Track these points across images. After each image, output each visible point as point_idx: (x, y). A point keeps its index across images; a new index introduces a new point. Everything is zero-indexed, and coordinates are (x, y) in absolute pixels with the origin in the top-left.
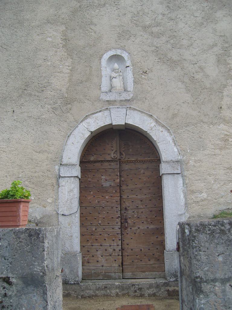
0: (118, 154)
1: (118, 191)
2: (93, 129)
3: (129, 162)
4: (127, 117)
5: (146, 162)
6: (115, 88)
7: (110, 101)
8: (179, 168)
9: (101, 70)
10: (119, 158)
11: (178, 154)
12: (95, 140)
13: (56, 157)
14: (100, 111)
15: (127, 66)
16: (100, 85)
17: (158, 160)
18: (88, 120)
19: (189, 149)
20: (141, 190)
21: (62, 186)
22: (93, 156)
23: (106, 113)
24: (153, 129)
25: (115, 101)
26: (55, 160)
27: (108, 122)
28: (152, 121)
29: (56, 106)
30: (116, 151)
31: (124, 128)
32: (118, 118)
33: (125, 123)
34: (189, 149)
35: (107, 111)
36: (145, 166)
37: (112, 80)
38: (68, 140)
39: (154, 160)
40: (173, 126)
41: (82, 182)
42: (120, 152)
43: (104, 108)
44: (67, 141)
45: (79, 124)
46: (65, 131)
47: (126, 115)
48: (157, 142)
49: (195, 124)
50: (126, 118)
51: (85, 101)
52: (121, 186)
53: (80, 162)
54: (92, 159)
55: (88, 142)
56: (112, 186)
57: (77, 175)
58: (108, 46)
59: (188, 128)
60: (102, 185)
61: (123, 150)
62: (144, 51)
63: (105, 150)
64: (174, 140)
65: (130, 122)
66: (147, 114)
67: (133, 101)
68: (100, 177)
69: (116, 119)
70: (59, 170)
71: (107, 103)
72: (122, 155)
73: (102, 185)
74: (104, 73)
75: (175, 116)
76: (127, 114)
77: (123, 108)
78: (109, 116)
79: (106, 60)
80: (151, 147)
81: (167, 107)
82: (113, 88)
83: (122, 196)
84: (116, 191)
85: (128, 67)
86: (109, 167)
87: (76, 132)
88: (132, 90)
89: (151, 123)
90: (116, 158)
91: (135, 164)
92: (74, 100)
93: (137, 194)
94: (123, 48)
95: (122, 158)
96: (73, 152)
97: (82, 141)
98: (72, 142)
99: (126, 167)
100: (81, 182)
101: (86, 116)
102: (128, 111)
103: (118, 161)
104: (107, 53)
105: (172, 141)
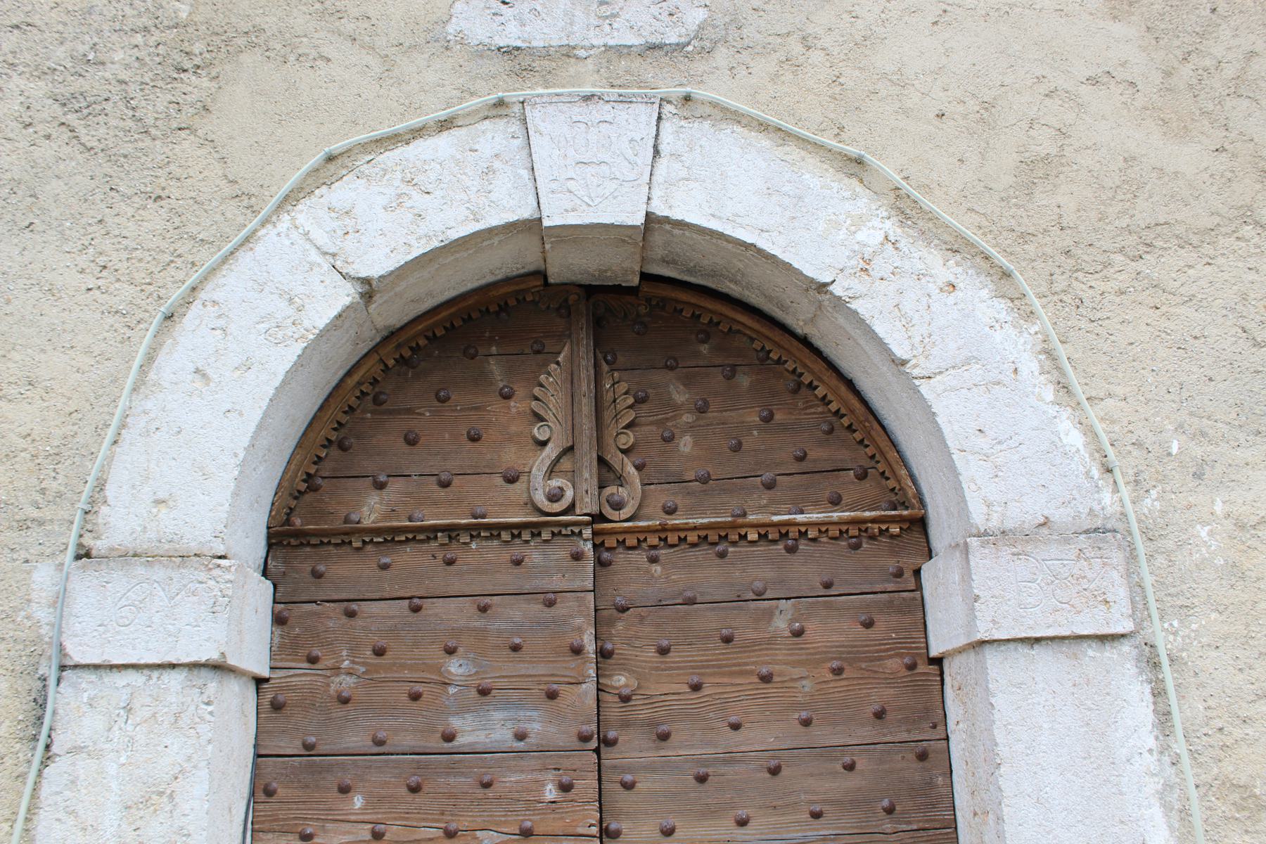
0: (589, 475)
1: (586, 785)
2: (377, 264)
3: (673, 538)
5: (814, 540)
8: (1120, 593)
10: (594, 509)
11: (1096, 473)
12: (402, 361)
13: (43, 491)
14: (445, 125)
17: (904, 525)
18: (345, 192)
19: (1180, 428)
20: (775, 771)
21: (75, 750)
22: (381, 486)
23: (495, 137)
24: (880, 267)
25: (568, 52)
26: (35, 514)
27: (509, 206)
28: (864, 202)
29: (93, 83)
30: (570, 450)
31: (623, 267)
32: (590, 177)
34: (1180, 428)
35: (501, 123)
36: (807, 569)
38: (165, 349)
39: (875, 528)
40: (1030, 248)
41: (277, 706)
42: (601, 461)
43: (474, 102)
44: (150, 358)
45: (263, 224)
46: (139, 276)
47: (656, 152)
48: (916, 372)
49: (1195, 240)
51: (326, 51)
52: (611, 743)
53: (269, 536)
54: (371, 510)
55: (349, 373)
56: (532, 740)
57: (214, 656)
59: (1148, 266)
60: (449, 737)
61: (628, 439)
63: (474, 439)
64: (1049, 353)
66: (818, 146)
68: (438, 669)
69: (571, 184)
70: (60, 601)
71: (498, 65)
72: (620, 480)
73: (449, 737)
75: (1037, 171)
76: (661, 147)
77: (624, 100)
80: (845, 421)
81: (972, 105)
83: (613, 826)
84: (565, 788)
86: (509, 579)
87: (232, 286)
89: (859, 222)
90: (570, 509)
91: (722, 555)
92: (241, 41)
93: (742, 813)
95: (618, 506)
96: (206, 433)
97: (284, 358)
98: (191, 368)
99: (637, 575)
100: (272, 701)
101: (330, 159)
102: (666, 126)
103: (587, 533)
105: (1035, 366)
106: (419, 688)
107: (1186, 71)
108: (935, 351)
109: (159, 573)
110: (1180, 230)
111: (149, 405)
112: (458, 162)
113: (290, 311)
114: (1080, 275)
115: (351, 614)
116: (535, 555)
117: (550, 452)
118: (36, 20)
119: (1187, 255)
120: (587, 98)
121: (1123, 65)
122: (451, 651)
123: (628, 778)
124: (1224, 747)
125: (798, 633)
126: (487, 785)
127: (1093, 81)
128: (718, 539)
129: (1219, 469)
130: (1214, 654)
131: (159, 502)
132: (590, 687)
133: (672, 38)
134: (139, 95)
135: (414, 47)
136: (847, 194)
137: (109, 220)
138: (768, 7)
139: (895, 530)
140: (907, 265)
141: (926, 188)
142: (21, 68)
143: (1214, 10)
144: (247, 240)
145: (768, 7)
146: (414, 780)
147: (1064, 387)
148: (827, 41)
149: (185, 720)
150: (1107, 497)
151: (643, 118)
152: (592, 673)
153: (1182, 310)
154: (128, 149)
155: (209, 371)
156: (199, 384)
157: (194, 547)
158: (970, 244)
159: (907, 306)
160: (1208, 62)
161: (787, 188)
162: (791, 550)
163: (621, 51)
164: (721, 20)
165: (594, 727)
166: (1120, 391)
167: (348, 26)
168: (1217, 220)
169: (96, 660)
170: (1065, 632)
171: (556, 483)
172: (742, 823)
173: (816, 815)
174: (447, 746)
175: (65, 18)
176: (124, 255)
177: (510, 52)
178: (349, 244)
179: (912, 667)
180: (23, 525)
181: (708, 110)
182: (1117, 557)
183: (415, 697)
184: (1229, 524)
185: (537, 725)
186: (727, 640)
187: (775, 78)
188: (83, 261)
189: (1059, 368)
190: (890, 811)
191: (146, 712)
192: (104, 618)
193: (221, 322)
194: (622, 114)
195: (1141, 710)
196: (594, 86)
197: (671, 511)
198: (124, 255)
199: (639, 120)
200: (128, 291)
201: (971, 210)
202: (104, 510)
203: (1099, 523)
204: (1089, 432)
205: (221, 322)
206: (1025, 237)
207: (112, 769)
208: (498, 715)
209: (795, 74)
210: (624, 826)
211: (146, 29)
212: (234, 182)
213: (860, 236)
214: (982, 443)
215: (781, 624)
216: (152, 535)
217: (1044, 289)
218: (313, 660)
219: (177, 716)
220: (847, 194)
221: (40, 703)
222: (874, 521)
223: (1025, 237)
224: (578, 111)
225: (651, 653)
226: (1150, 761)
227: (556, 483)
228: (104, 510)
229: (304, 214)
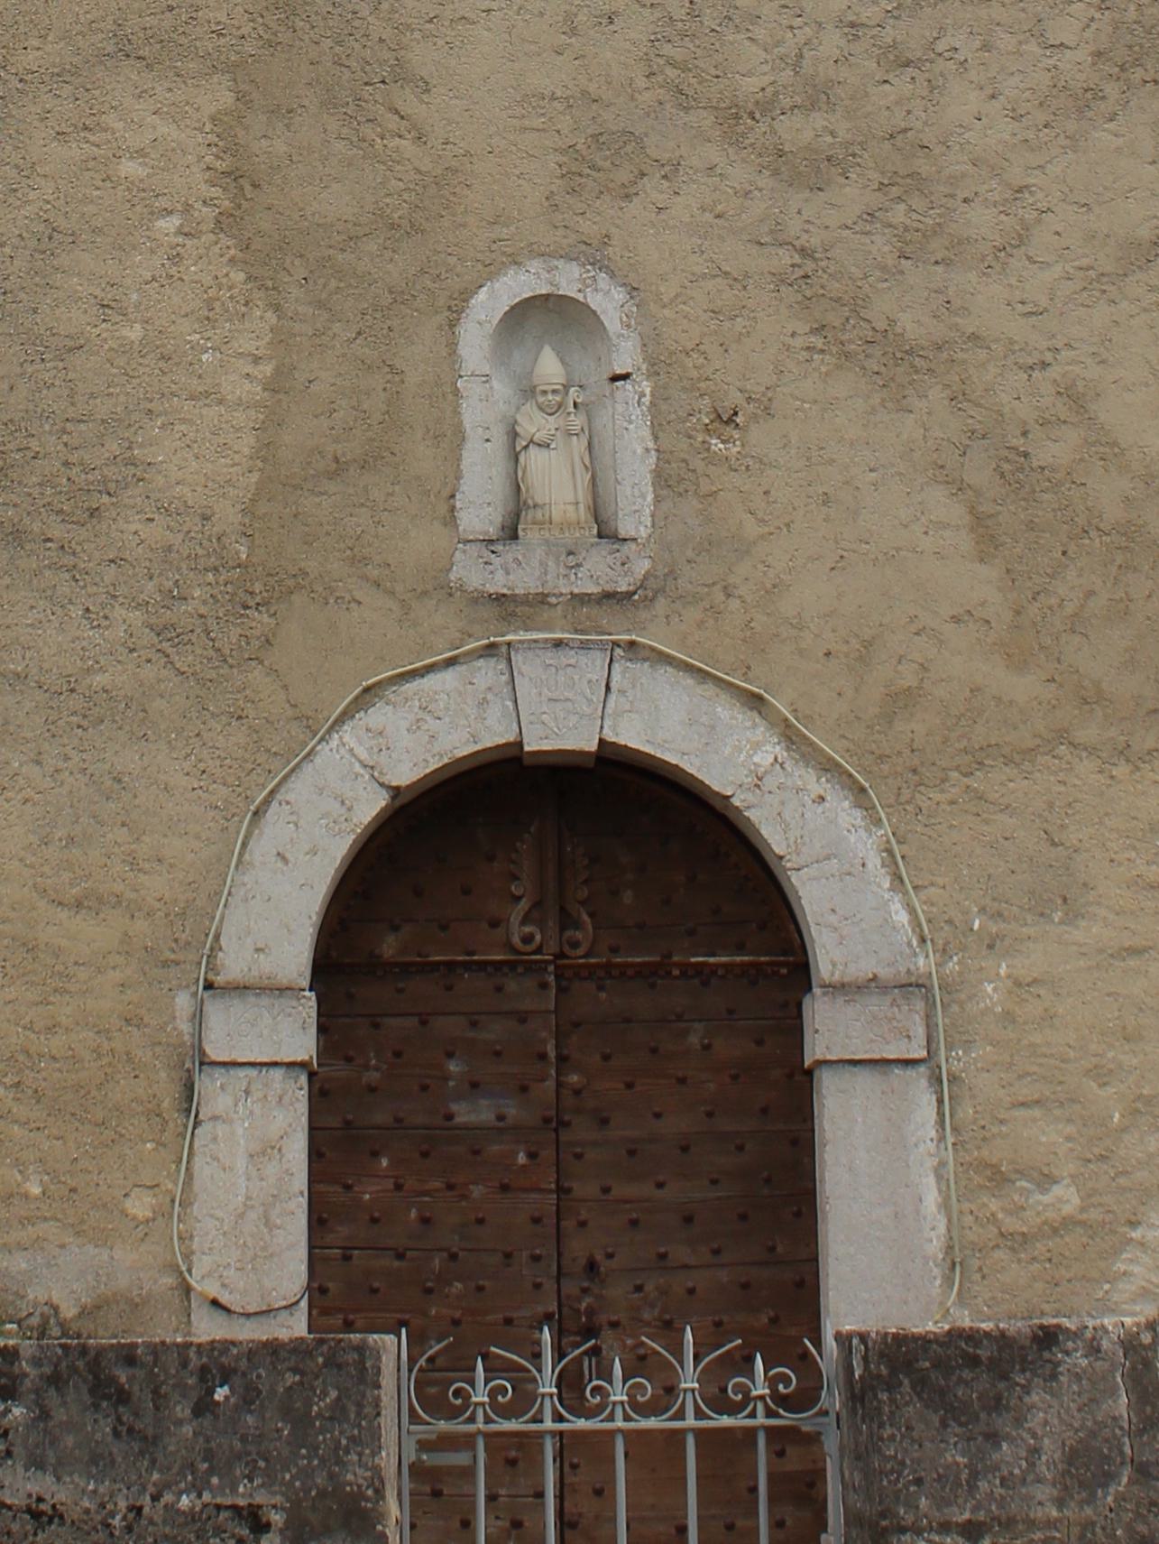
1: (548, 1153)
8: (920, 1031)
9: (456, 393)
11: (915, 943)
13: (176, 940)
14: (451, 662)
16: (453, 496)
18: (377, 715)
19: (982, 910)
20: (685, 1149)
21: (215, 1118)
22: (396, 928)
23: (487, 673)
24: (770, 783)
25: (542, 599)
26: (173, 957)
27: (494, 733)
32: (561, 708)
34: (982, 910)
37: (522, 459)
40: (885, 767)
42: (562, 909)
46: (230, 780)
49: (1017, 758)
50: (609, 710)
51: (358, 595)
52: (567, 1124)
54: (389, 947)
63: (466, 892)
64: (890, 852)
70: (198, 1017)
72: (577, 925)
76: (613, 685)
77: (585, 646)
78: (506, 690)
79: (489, 328)
82: (531, 513)
85: (625, 377)
87: (299, 789)
89: (757, 746)
90: (539, 951)
91: (653, 986)
92: (291, 583)
93: (661, 1178)
94: (594, 254)
95: (575, 945)
101: (367, 690)
102: (616, 667)
103: (551, 968)
106: (428, 1081)
107: (1033, 610)
108: (804, 849)
109: (265, 1001)
110: (1006, 750)
111: (246, 879)
112: (460, 693)
113: (343, 810)
114: (922, 788)
115: (376, 1026)
116: (512, 986)
117: (524, 905)
118: (127, 555)
119: (1010, 771)
120: (558, 644)
121: (982, 604)
122: (450, 1055)
123: (578, 1150)
124: (984, 1139)
125: (707, 1047)
126: (476, 1153)
127: (956, 619)
128: (649, 974)
129: (1007, 941)
130: (986, 1075)
131: (258, 950)
132: (550, 1084)
133: (623, 587)
134: (216, 627)
135: (425, 593)
136: (748, 724)
137: (204, 734)
138: (699, 559)
139: (784, 971)
140: (789, 783)
141: (808, 720)
142: (121, 600)
143: (1064, 553)
144: (309, 754)
145: (699, 559)
146: (425, 1147)
147: (897, 878)
148: (742, 591)
149: (286, 1099)
150: (921, 961)
151: (598, 662)
152: (553, 1072)
153: (999, 817)
154: (213, 674)
155: (288, 855)
156: (280, 864)
157: (285, 982)
158: (838, 765)
159: (787, 815)
160: (1053, 601)
161: (704, 719)
162: (705, 984)
163: (581, 599)
164: (662, 570)
165: (553, 1113)
166: (940, 881)
167: (374, 573)
168: (1038, 741)
169: (227, 1059)
170: (877, 1056)
171: (527, 929)
172: (660, 1185)
173: (714, 1182)
174: (448, 1124)
175: (150, 555)
176: (218, 763)
177: (500, 598)
178: (383, 758)
179: (790, 1076)
180: (166, 964)
181: (647, 653)
182: (920, 1005)
183: (424, 1088)
184: (1009, 983)
185: (512, 1111)
186: (654, 1051)
187: (700, 624)
188: (187, 765)
189: (896, 864)
190: (768, 1180)
191: (260, 1094)
192: (233, 1031)
193: (294, 818)
194: (583, 659)
195: (931, 1113)
196: (563, 631)
197: (614, 950)
198: (218, 763)
199: (594, 665)
200: (224, 791)
201: (843, 736)
202: (220, 954)
203: (913, 979)
204: (912, 911)
205: (294, 818)
206: (882, 758)
207: (240, 1131)
208: (484, 1102)
209: (716, 620)
210: (575, 1185)
211: (216, 569)
212: (295, 706)
213: (756, 759)
214: (833, 919)
215: (694, 1040)
216: (255, 973)
217: (892, 801)
218: (349, 1059)
219: (280, 1099)
220: (748, 724)
221: (189, 1087)
222: (768, 964)
223: (882, 758)
224: (550, 657)
225: (597, 1057)
226: (932, 1147)
227: (527, 929)
228: (220, 954)
229: (348, 733)
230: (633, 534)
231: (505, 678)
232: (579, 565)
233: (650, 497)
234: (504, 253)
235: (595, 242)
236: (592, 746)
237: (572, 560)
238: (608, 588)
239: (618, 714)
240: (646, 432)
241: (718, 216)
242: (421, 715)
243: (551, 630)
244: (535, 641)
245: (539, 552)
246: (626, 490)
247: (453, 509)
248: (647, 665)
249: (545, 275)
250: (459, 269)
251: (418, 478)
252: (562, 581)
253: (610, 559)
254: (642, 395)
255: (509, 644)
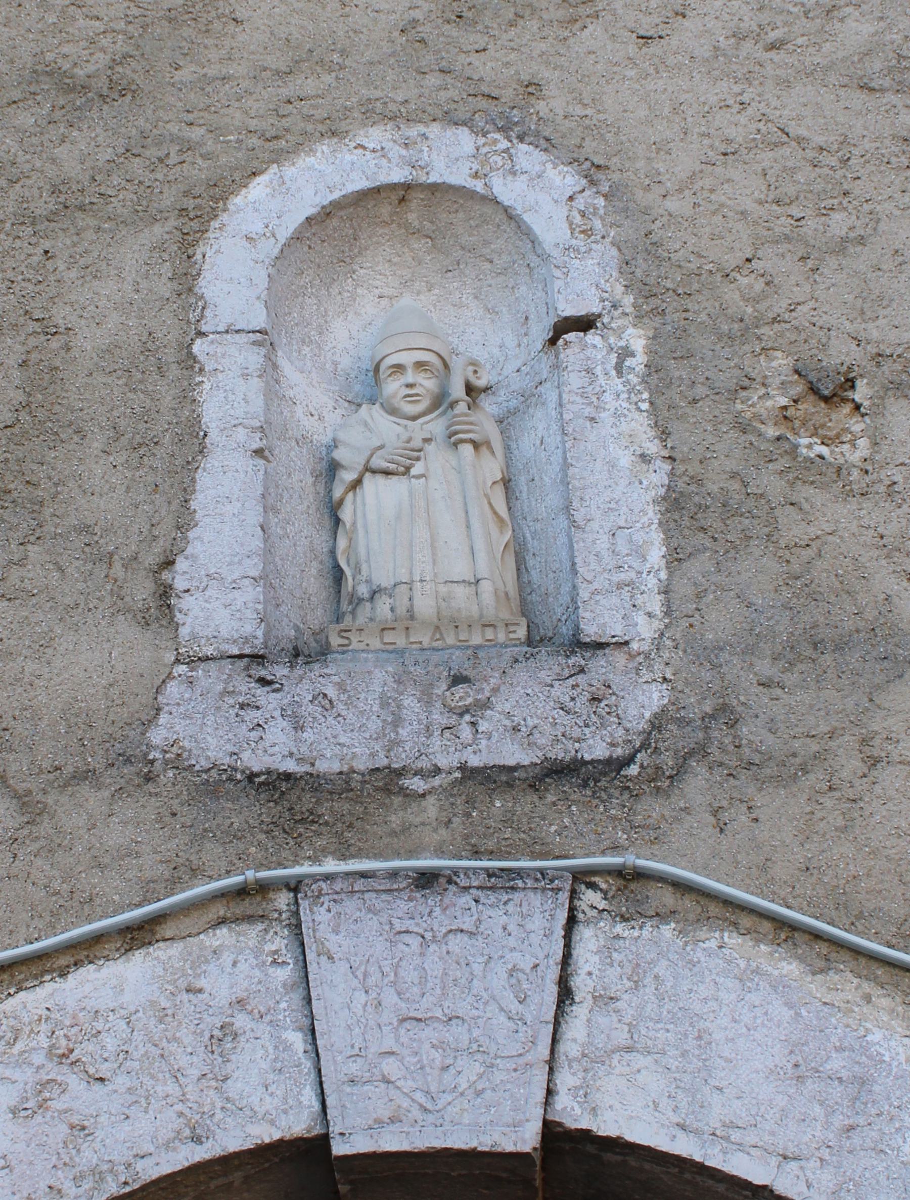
4: (576, 1029)
6: (383, 607)
7: (314, 782)
9: (189, 362)
14: (138, 935)
15: (569, 311)
16: (169, 563)
23: (237, 962)
25: (388, 781)
27: (262, 1108)
33: (552, 1132)
37: (346, 514)
47: (565, 994)
50: (569, 1047)
58: (310, 86)
62: (799, 140)
65: (629, 1109)
67: (663, 781)
69: (390, 1067)
71: (241, 813)
74: (228, 397)
76: (581, 983)
77: (504, 882)
78: (288, 1006)
79: (270, 248)
82: (365, 611)
85: (585, 324)
88: (645, 630)
94: (509, 116)
102: (588, 940)
104: (289, 171)
112: (162, 1016)
120: (426, 880)
133: (596, 749)
145: (791, 679)
151: (537, 923)
161: (836, 1063)
164: (697, 706)
177: (273, 785)
194: (496, 915)
196: (440, 852)
199: (526, 927)
224: (401, 907)
230: (616, 629)
231: (284, 974)
232: (485, 705)
233: (656, 554)
234: (308, 118)
235: (507, 95)
236: (525, 1138)
237: (463, 695)
238: (558, 753)
239: (593, 1059)
240: (639, 425)
241: (773, 47)
242: (53, 1071)
243: (411, 854)
244: (364, 875)
245: (381, 678)
246: (595, 543)
247: (165, 593)
248: (668, 930)
249: (396, 151)
250: (210, 146)
251: (86, 529)
252: (436, 742)
253: (561, 692)
254: (626, 353)
255: (295, 886)
